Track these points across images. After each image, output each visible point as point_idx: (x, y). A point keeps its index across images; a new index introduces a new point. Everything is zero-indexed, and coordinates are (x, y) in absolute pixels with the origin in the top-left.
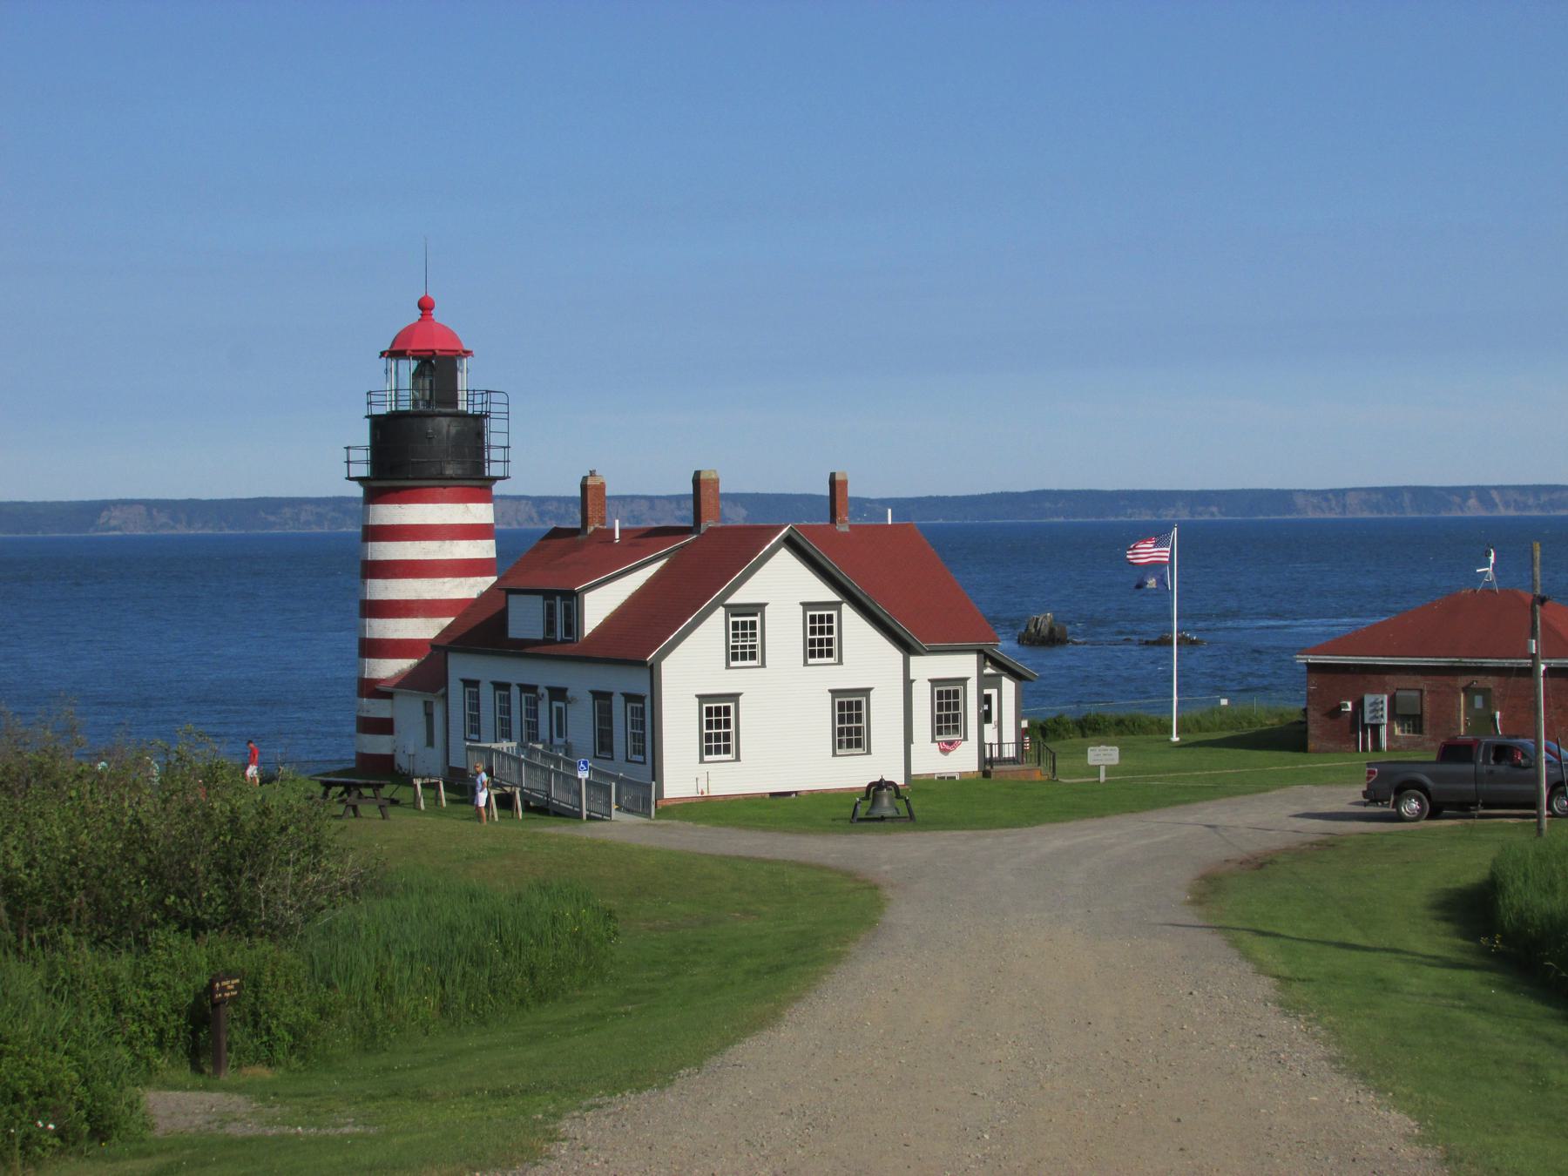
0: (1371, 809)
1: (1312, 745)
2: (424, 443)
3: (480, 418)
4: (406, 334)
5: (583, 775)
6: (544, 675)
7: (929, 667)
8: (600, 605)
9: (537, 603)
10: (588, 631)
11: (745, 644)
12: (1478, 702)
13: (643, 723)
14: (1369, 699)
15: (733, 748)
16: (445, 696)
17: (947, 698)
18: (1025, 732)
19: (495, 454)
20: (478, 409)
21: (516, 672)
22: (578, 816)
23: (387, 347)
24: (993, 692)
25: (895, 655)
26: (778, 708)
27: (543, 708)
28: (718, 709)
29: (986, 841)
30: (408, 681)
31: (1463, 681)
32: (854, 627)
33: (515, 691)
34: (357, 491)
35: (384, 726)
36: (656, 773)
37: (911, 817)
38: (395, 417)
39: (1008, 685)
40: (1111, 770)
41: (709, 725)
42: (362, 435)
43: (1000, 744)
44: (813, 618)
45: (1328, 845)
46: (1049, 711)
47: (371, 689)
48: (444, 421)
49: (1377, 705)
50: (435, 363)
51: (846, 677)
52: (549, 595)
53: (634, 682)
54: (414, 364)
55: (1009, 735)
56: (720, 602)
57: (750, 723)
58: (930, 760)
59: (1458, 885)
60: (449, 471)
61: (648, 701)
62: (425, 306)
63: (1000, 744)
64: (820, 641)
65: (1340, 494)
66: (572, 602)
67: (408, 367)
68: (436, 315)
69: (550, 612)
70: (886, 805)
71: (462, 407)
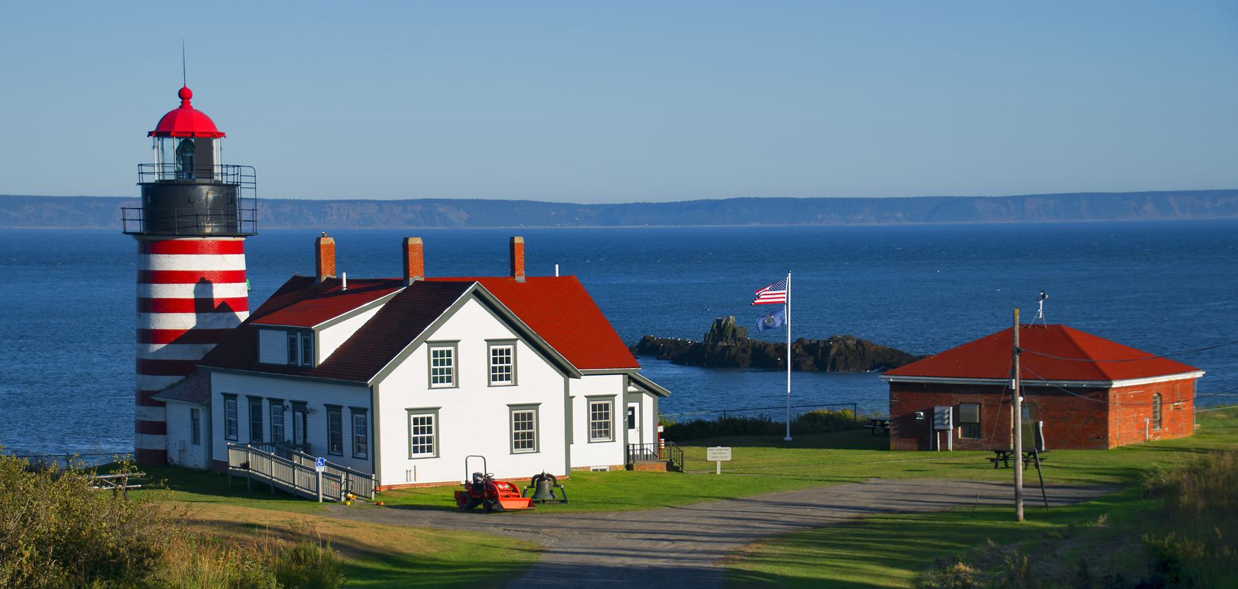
1: (893, 444)
3: (233, 186)
6: (289, 391)
8: (332, 338)
9: (282, 337)
10: (322, 360)
11: (443, 370)
13: (365, 429)
15: (513, 377)
16: (209, 406)
18: (661, 435)
19: (246, 215)
20: (231, 179)
21: (266, 388)
22: (316, 499)
23: (153, 129)
24: (636, 405)
25: (558, 378)
27: (288, 416)
28: (422, 419)
32: (526, 357)
34: (134, 243)
38: (162, 185)
39: (648, 401)
41: (416, 431)
43: (641, 444)
44: (495, 352)
46: (675, 418)
48: (205, 189)
50: (186, 129)
51: (520, 394)
52: (291, 331)
54: (176, 142)
55: (649, 438)
59: (358, 538)
60: (208, 230)
61: (369, 413)
62: (185, 94)
63: (641, 444)
64: (501, 368)
65: (1020, 200)
67: (172, 144)
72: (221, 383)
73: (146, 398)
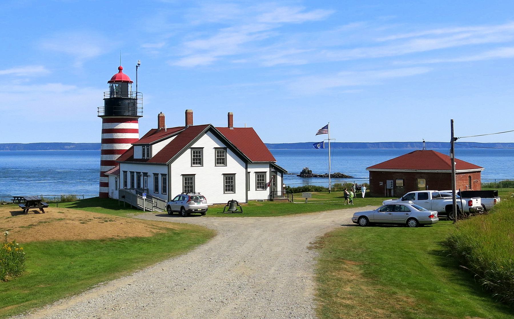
2: (118, 107)
4: (114, 78)
7: (252, 170)
8: (157, 148)
11: (197, 158)
17: (260, 176)
27: (142, 178)
32: (230, 159)
33: (135, 174)
42: (102, 104)
50: (120, 84)
51: (227, 170)
52: (143, 145)
62: (120, 69)
69: (144, 150)
70: (234, 208)
71: (129, 96)
72: (124, 167)
73: (103, 174)
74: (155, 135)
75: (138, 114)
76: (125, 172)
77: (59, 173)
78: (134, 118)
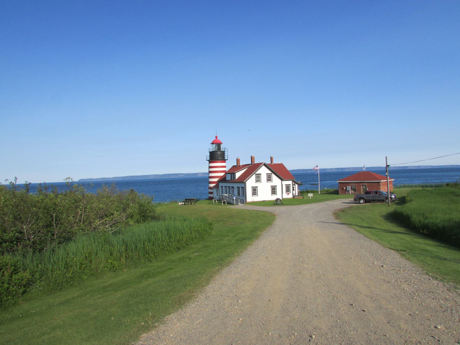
0: (356, 202)
2: (216, 156)
4: (214, 141)
5: (235, 198)
6: (231, 185)
7: (285, 183)
8: (238, 175)
11: (258, 179)
12: (364, 187)
14: (348, 187)
17: (288, 187)
25: (280, 181)
26: (262, 189)
29: (295, 207)
30: (214, 187)
31: (362, 184)
32: (274, 177)
35: (212, 193)
36: (246, 198)
37: (282, 204)
38: (213, 152)
39: (296, 185)
40: (312, 197)
42: (208, 154)
45: (351, 208)
47: (210, 188)
49: (349, 188)
50: (218, 144)
51: (273, 184)
52: (231, 174)
53: (242, 185)
55: (297, 192)
56: (254, 173)
57: (259, 191)
58: (285, 196)
62: (216, 137)
64: (269, 179)
66: (234, 174)
68: (218, 138)
70: (279, 202)
74: (236, 168)
75: (226, 159)
76: (222, 187)
77: (393, 249)
78: (224, 160)
